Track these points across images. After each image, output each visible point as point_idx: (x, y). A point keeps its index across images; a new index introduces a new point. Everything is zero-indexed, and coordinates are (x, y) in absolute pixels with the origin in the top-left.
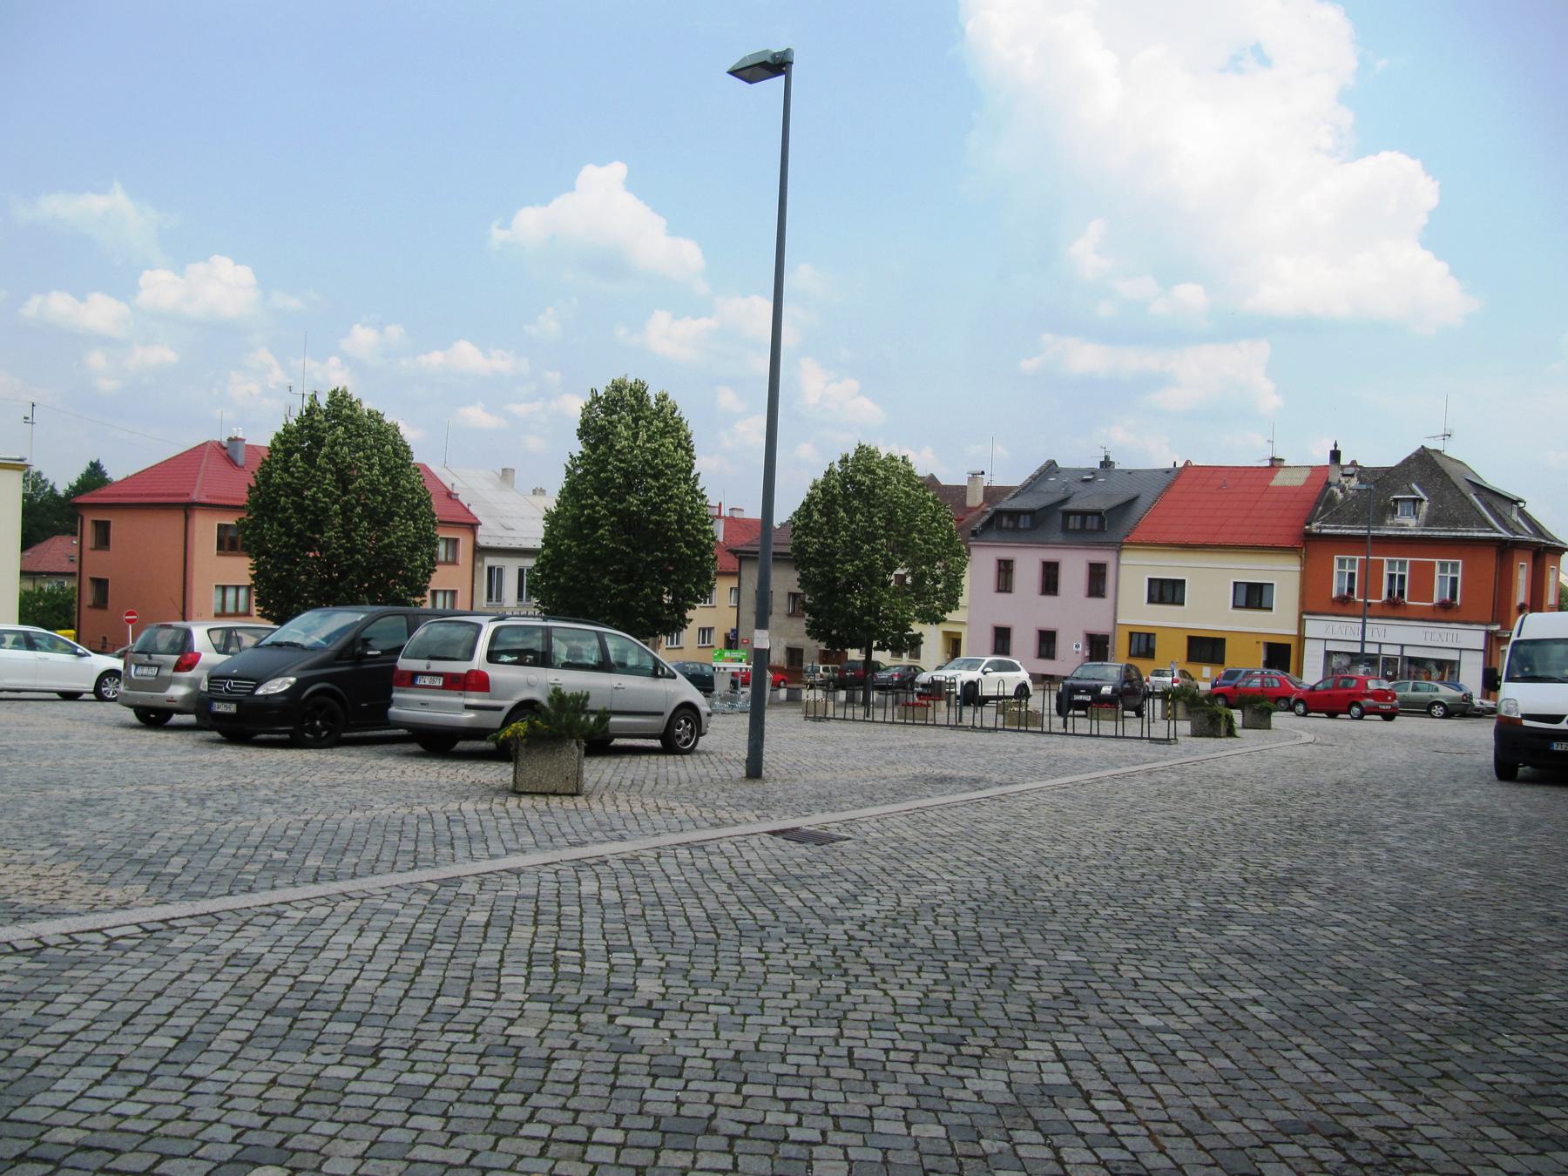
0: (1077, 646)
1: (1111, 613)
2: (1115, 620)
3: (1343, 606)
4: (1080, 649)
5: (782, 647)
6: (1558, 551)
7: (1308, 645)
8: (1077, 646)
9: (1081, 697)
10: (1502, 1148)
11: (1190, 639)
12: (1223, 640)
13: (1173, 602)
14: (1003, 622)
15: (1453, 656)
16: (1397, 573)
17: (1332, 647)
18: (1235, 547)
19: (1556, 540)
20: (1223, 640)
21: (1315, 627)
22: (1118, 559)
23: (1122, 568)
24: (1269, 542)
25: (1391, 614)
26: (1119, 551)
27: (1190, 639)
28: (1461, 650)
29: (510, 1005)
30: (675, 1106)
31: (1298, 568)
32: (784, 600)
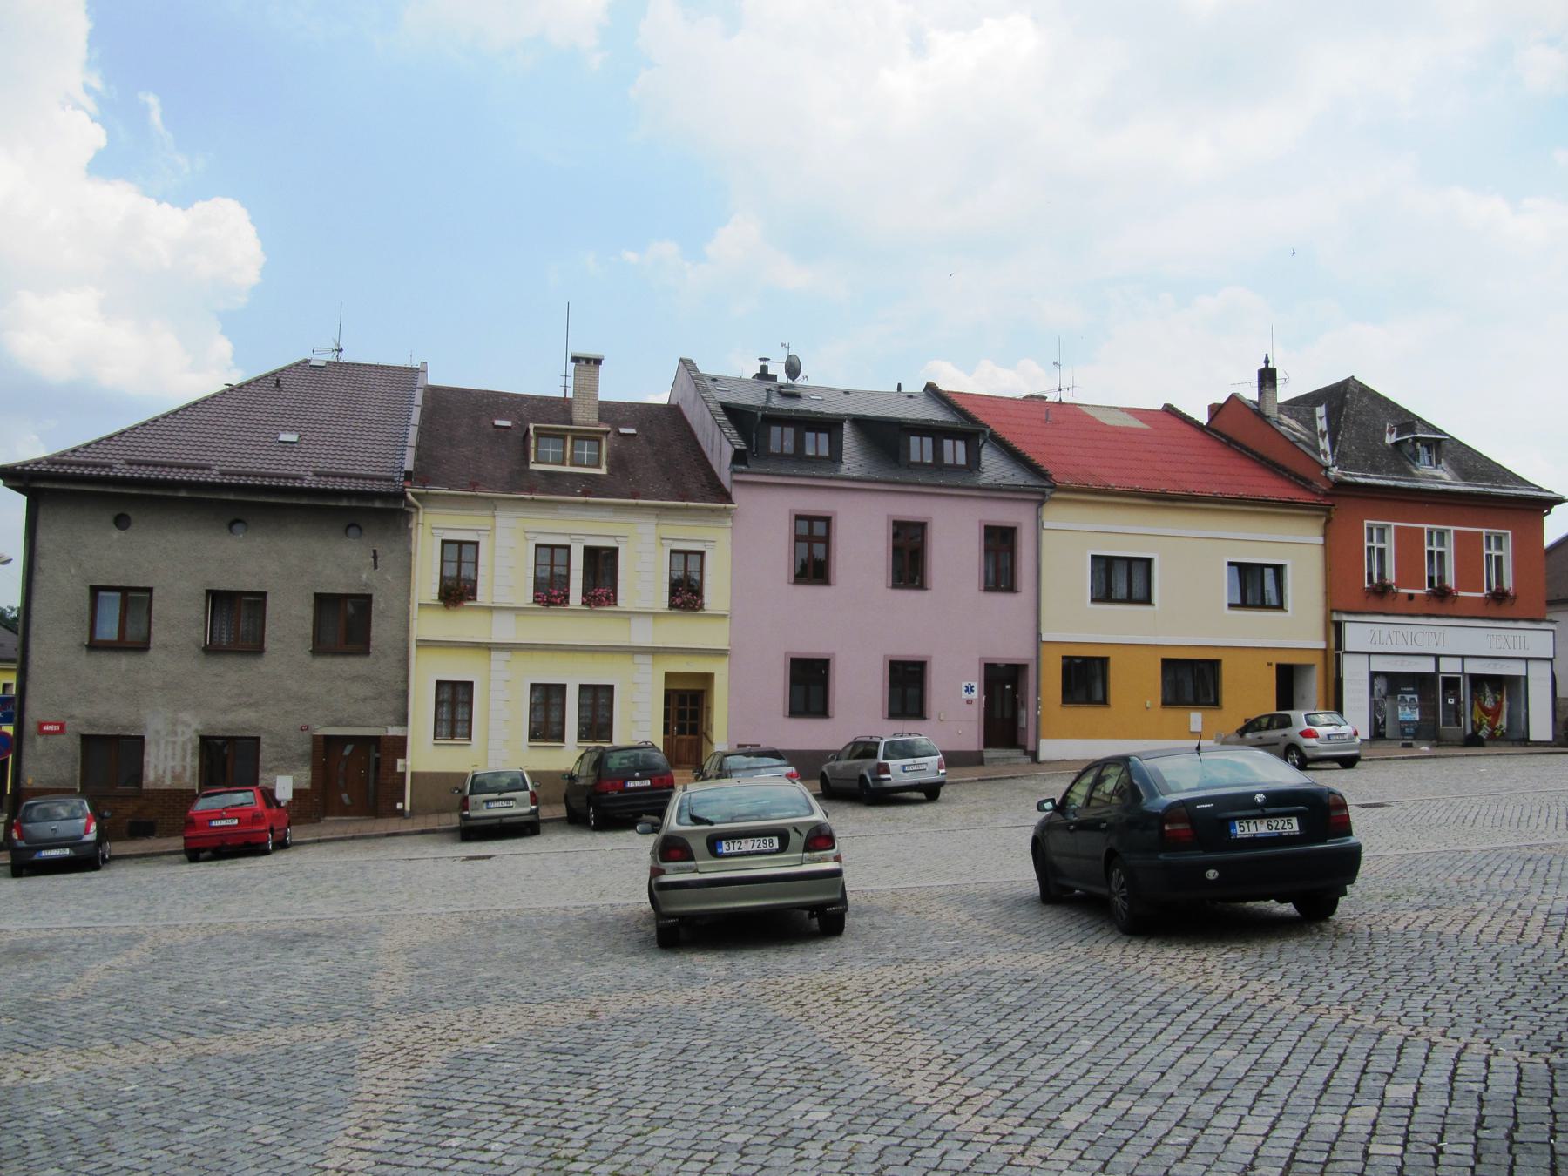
0: (969, 689)
1: (1031, 623)
2: (1039, 635)
3: (1380, 598)
4: (975, 695)
5: (191, 726)
6: (1547, 503)
7: (1348, 662)
8: (969, 689)
9: (638, 784)
10: (435, 1168)
11: (1167, 663)
12: (1104, 661)
13: (1130, 600)
14: (810, 648)
15: (1515, 669)
16: (1436, 549)
17: (1381, 665)
18: (1137, 494)
19: (1541, 489)
20: (1104, 661)
21: (1357, 634)
22: (1038, 518)
23: (1045, 536)
24: (1126, 484)
25: (1493, 614)
26: (1041, 503)
27: (1167, 663)
28: (1527, 659)
29: (1298, 1110)
30: (1551, 1116)
31: (1321, 540)
32: (196, 610)
